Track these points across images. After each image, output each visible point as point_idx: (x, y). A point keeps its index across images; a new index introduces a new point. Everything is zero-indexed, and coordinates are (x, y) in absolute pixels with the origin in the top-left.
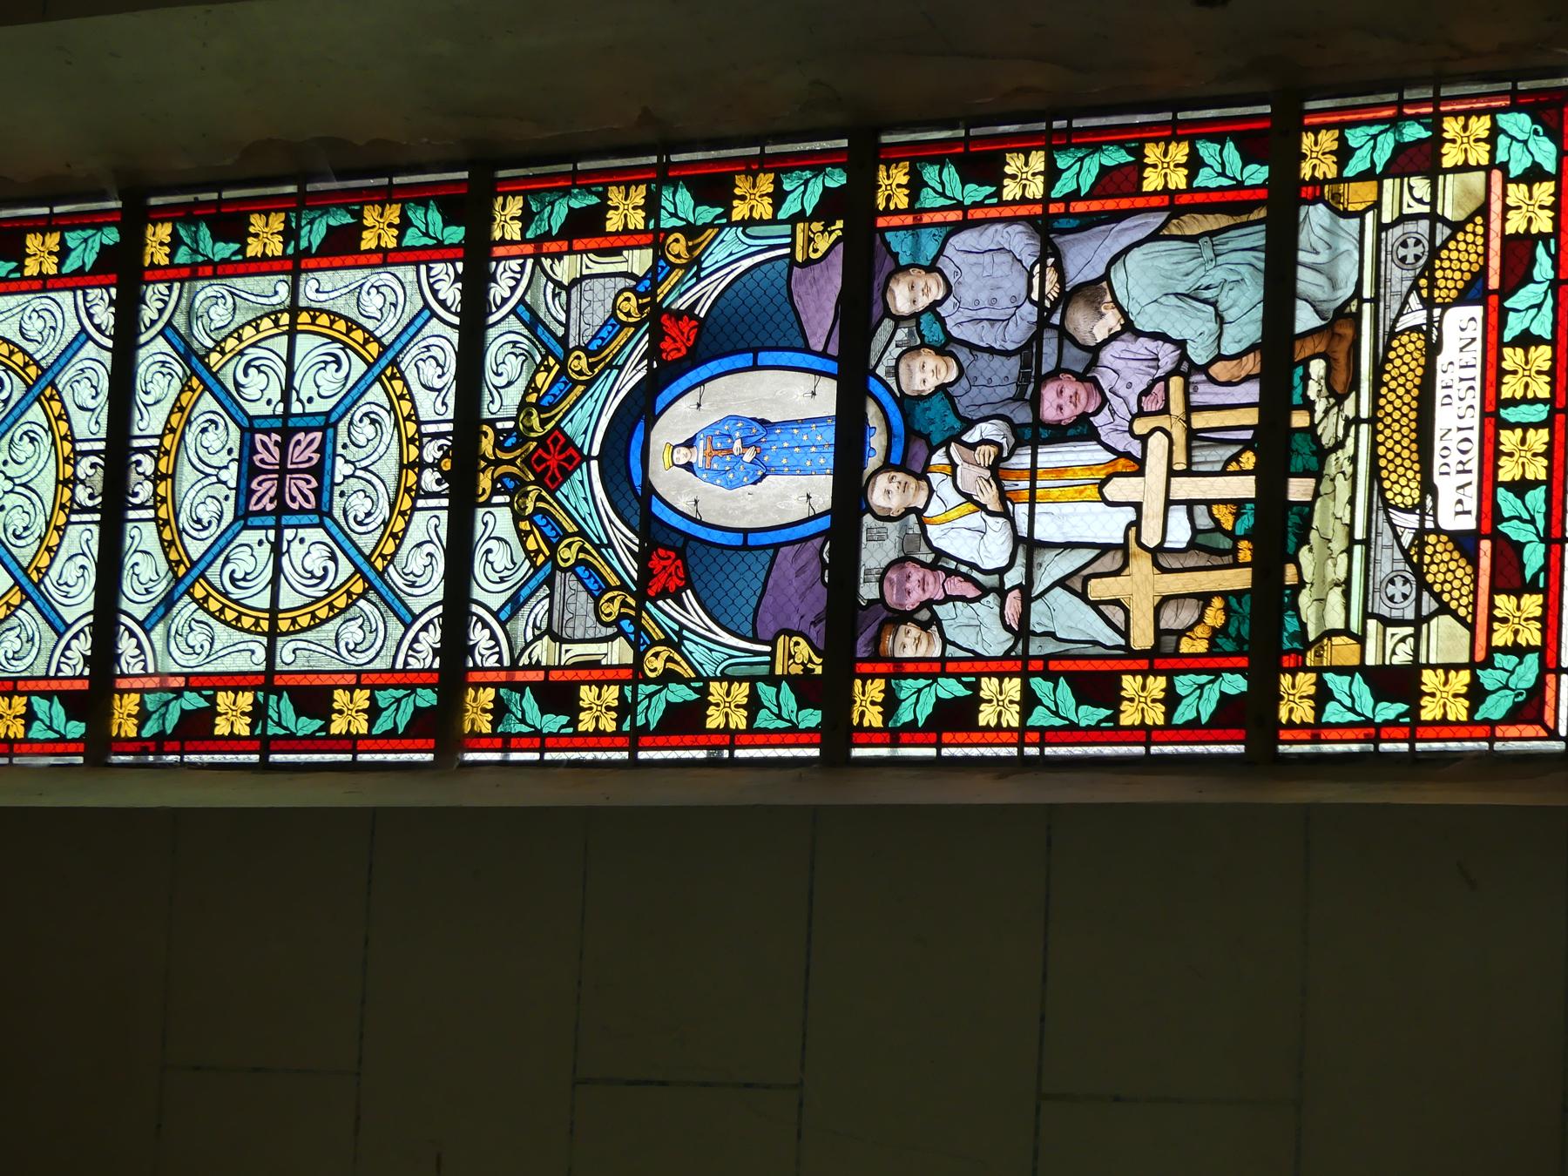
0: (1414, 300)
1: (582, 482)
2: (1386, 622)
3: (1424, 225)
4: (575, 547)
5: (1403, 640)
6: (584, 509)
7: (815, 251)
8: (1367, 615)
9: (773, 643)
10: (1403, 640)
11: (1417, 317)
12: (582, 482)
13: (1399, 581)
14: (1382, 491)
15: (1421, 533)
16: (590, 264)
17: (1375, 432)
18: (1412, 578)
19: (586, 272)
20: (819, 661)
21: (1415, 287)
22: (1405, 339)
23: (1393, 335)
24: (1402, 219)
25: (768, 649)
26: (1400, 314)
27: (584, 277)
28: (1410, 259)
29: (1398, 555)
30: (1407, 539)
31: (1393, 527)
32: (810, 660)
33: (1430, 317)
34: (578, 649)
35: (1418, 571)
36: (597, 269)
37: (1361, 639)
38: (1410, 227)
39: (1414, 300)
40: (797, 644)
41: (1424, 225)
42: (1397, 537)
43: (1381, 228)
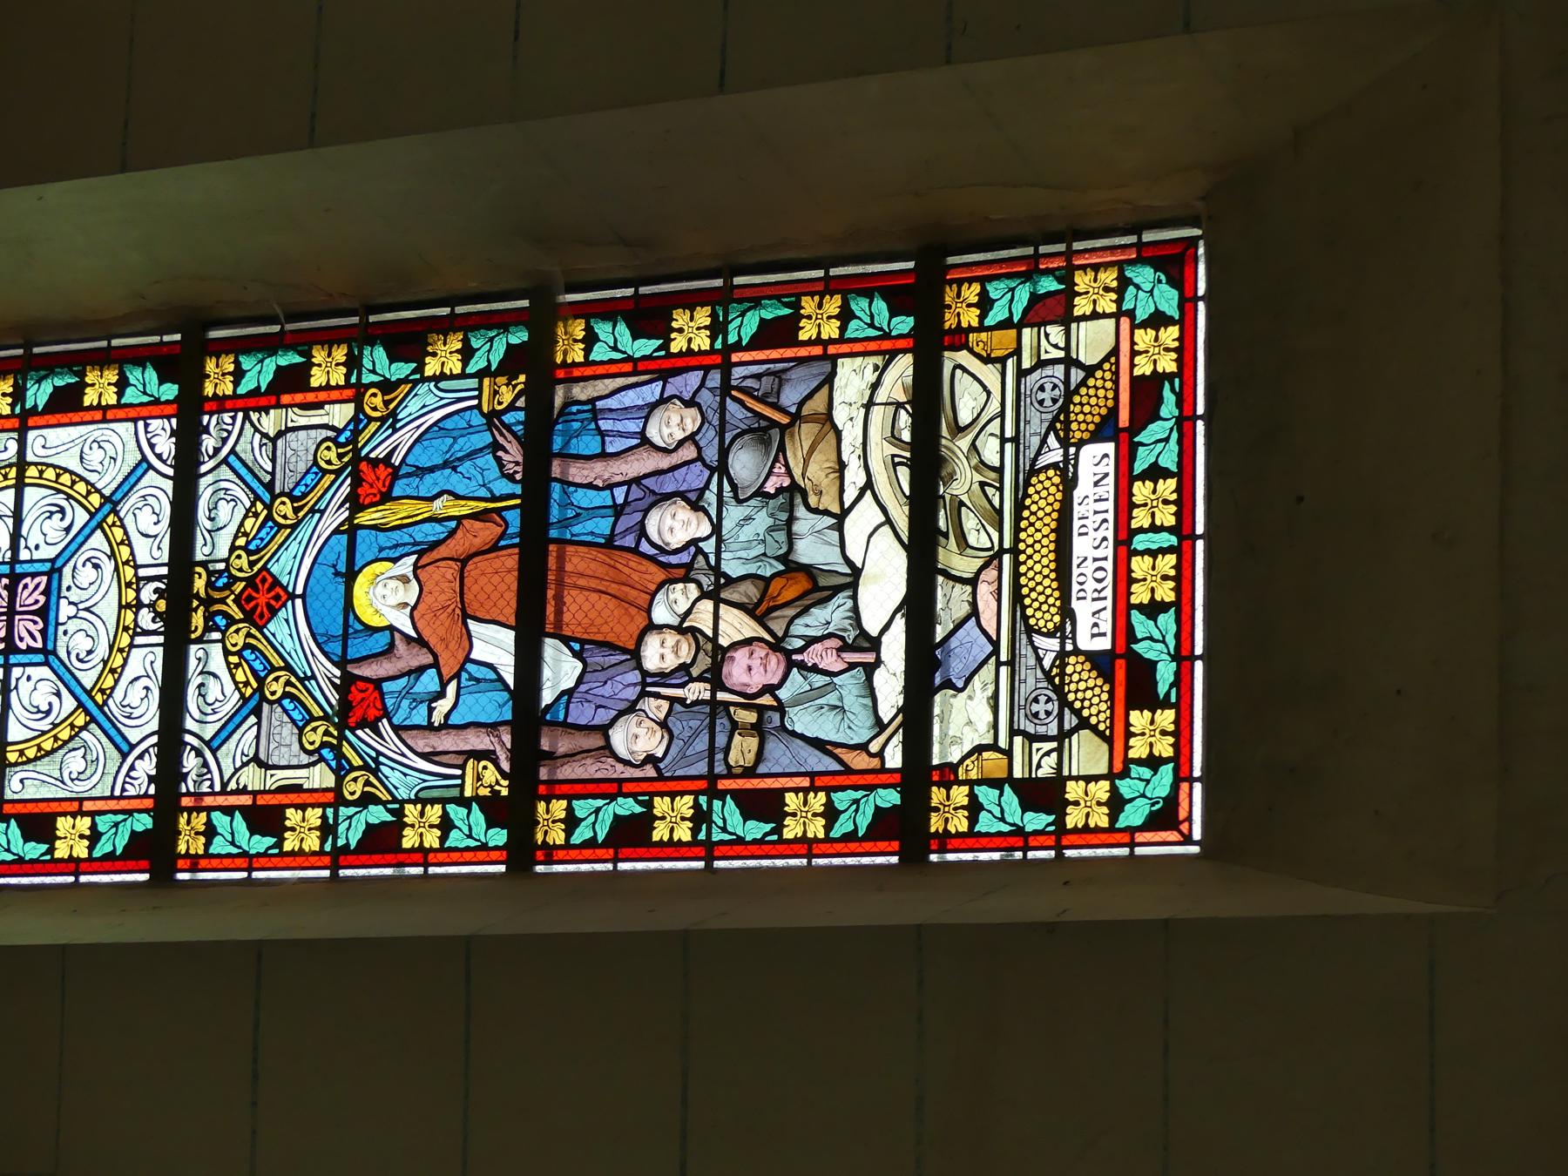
0: (1052, 441)
1: (287, 621)
2: (1031, 738)
3: (1059, 370)
4: (282, 680)
5: (1048, 754)
6: (288, 644)
7: (500, 403)
8: (1013, 732)
9: (463, 767)
10: (1048, 754)
11: (1055, 455)
12: (287, 621)
13: (1043, 699)
14: (1025, 618)
15: (1062, 655)
16: (295, 418)
17: (1016, 564)
18: (1054, 697)
19: (290, 425)
20: (505, 783)
21: (1051, 427)
22: (1042, 477)
23: (1033, 472)
24: (1041, 364)
25: (459, 772)
26: (1038, 453)
27: (289, 430)
28: (1048, 403)
29: (1040, 675)
30: (1047, 663)
31: (1035, 649)
32: (497, 783)
33: (1066, 454)
34: (280, 774)
35: (1060, 691)
36: (303, 422)
37: (1009, 753)
38: (1048, 371)
39: (1052, 441)
40: (485, 768)
41: (1059, 370)
42: (1039, 660)
43: (1021, 374)
